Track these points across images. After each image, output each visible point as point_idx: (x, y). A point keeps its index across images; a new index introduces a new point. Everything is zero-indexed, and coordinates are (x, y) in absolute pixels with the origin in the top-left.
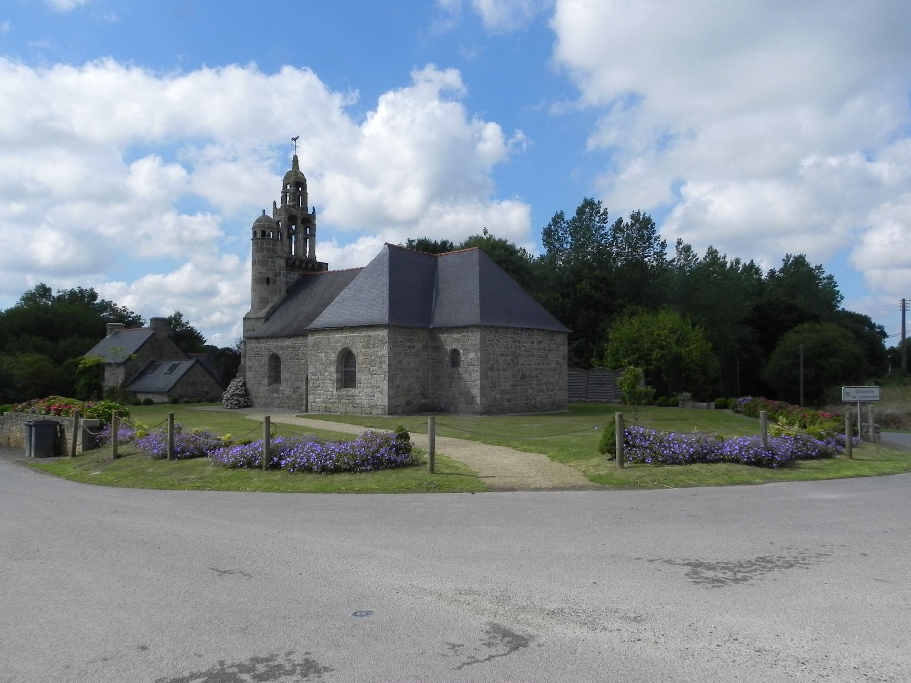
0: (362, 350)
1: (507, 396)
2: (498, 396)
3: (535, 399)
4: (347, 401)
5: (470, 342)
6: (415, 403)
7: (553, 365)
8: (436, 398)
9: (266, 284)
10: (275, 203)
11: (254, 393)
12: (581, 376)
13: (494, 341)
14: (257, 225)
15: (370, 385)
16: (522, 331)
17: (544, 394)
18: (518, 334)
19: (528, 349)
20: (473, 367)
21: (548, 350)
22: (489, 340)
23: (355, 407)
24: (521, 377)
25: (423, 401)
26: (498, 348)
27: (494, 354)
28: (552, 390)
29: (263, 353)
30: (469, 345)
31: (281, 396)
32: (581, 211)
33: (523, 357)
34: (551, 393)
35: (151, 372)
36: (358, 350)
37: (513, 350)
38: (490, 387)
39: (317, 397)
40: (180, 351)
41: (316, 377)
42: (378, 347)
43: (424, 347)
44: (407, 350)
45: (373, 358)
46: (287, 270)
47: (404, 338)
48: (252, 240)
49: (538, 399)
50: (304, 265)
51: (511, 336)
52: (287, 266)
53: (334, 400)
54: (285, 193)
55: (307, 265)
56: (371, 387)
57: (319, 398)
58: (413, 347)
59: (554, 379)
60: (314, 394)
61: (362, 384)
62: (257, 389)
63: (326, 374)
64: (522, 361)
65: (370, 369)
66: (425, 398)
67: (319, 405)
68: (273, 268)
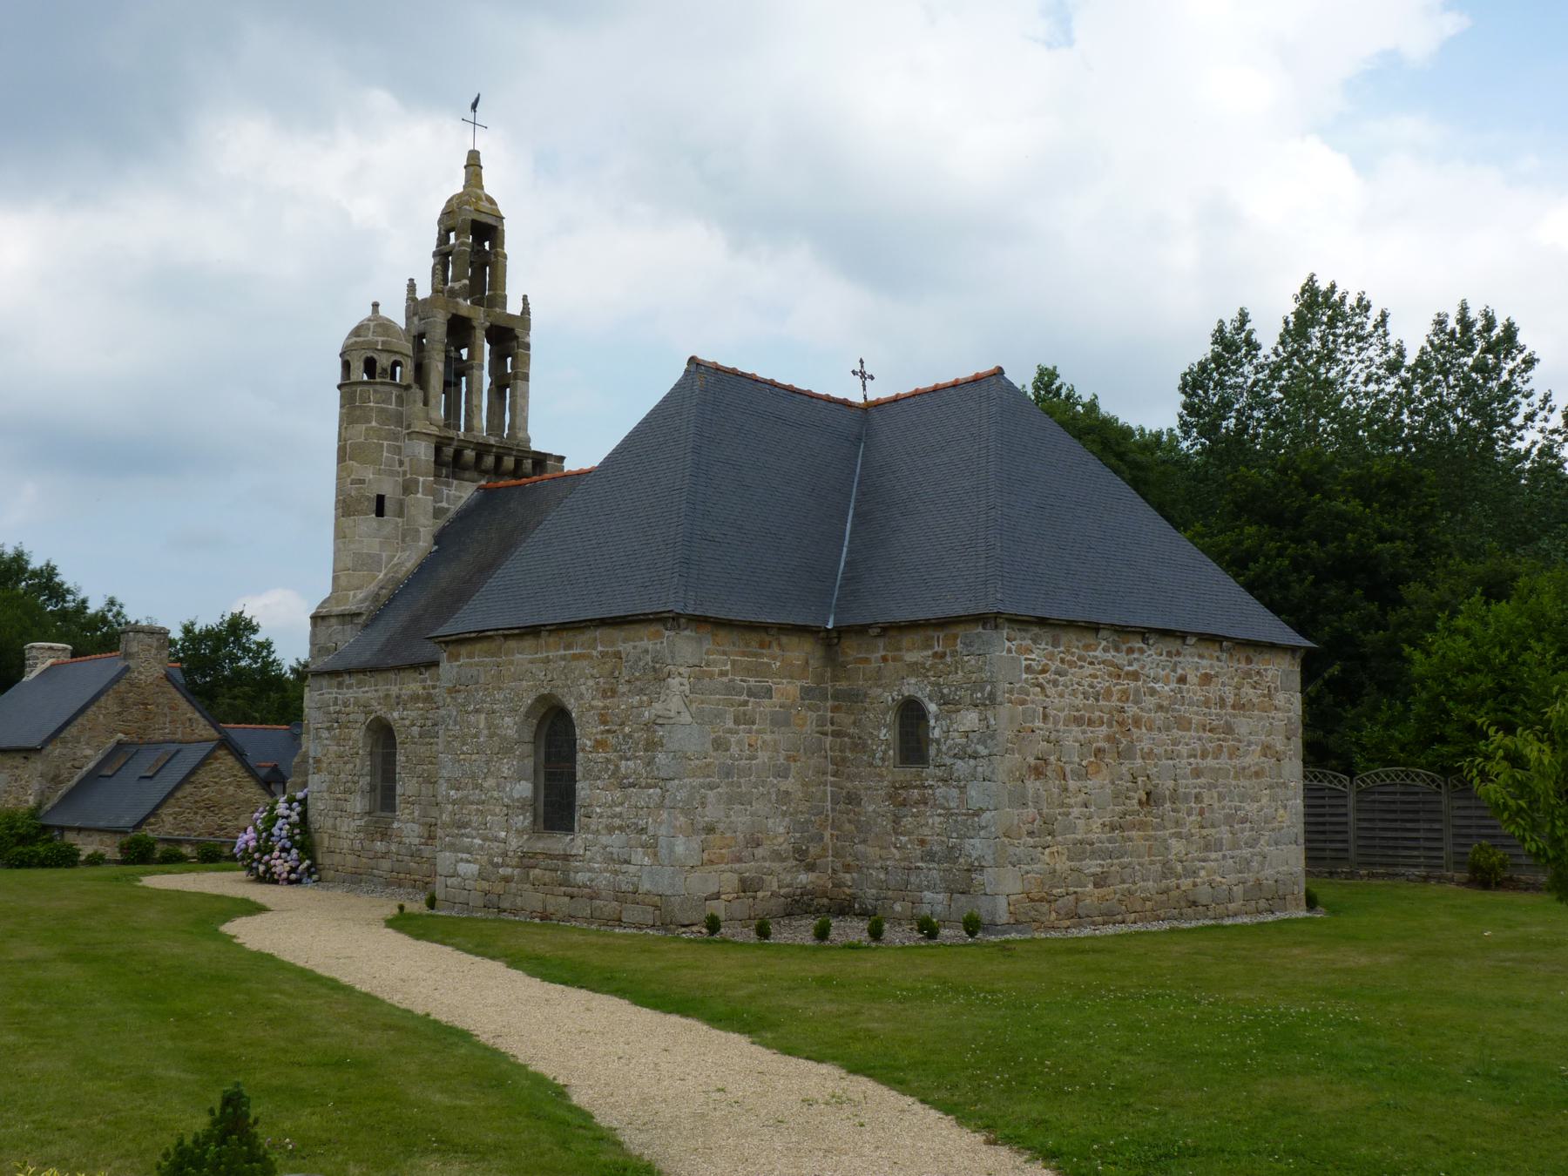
0: (595, 703)
1: (1093, 866)
2: (1062, 865)
3: (1195, 873)
4: (548, 876)
5: (960, 673)
6: (775, 887)
7: (1253, 759)
8: (847, 868)
9: (374, 515)
10: (412, 286)
11: (326, 836)
12: (1334, 793)
13: (1044, 671)
14: (352, 344)
15: (617, 822)
16: (1145, 640)
17: (1224, 857)
18: (1130, 651)
19: (1165, 703)
20: (972, 762)
21: (1233, 707)
22: (1028, 669)
23: (572, 897)
24: (1144, 798)
25: (804, 878)
26: (1061, 696)
27: (1045, 717)
28: (1253, 843)
29: (351, 717)
30: (960, 687)
31: (393, 848)
32: (1297, 330)
33: (1150, 729)
34: (1246, 852)
35: (110, 773)
36: (582, 701)
37: (1114, 702)
38: (1031, 834)
39: (462, 860)
40: (197, 715)
41: (460, 794)
42: (641, 691)
43: (806, 692)
44: (745, 703)
45: (627, 730)
46: (437, 475)
47: (734, 663)
48: (339, 387)
49: (1203, 873)
50: (489, 461)
51: (1108, 656)
52: (438, 462)
53: (510, 870)
54: (443, 255)
55: (499, 459)
56: (621, 828)
57: (468, 861)
58: (768, 693)
59: (1256, 805)
60: (453, 847)
61: (594, 820)
62: (335, 828)
63: (491, 782)
64: (1145, 745)
65: (617, 766)
66: (811, 868)
67: (470, 884)
68: (397, 468)
